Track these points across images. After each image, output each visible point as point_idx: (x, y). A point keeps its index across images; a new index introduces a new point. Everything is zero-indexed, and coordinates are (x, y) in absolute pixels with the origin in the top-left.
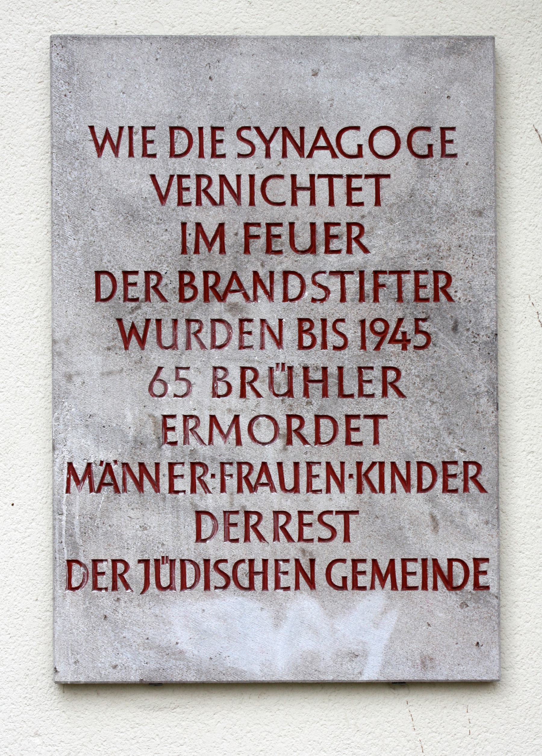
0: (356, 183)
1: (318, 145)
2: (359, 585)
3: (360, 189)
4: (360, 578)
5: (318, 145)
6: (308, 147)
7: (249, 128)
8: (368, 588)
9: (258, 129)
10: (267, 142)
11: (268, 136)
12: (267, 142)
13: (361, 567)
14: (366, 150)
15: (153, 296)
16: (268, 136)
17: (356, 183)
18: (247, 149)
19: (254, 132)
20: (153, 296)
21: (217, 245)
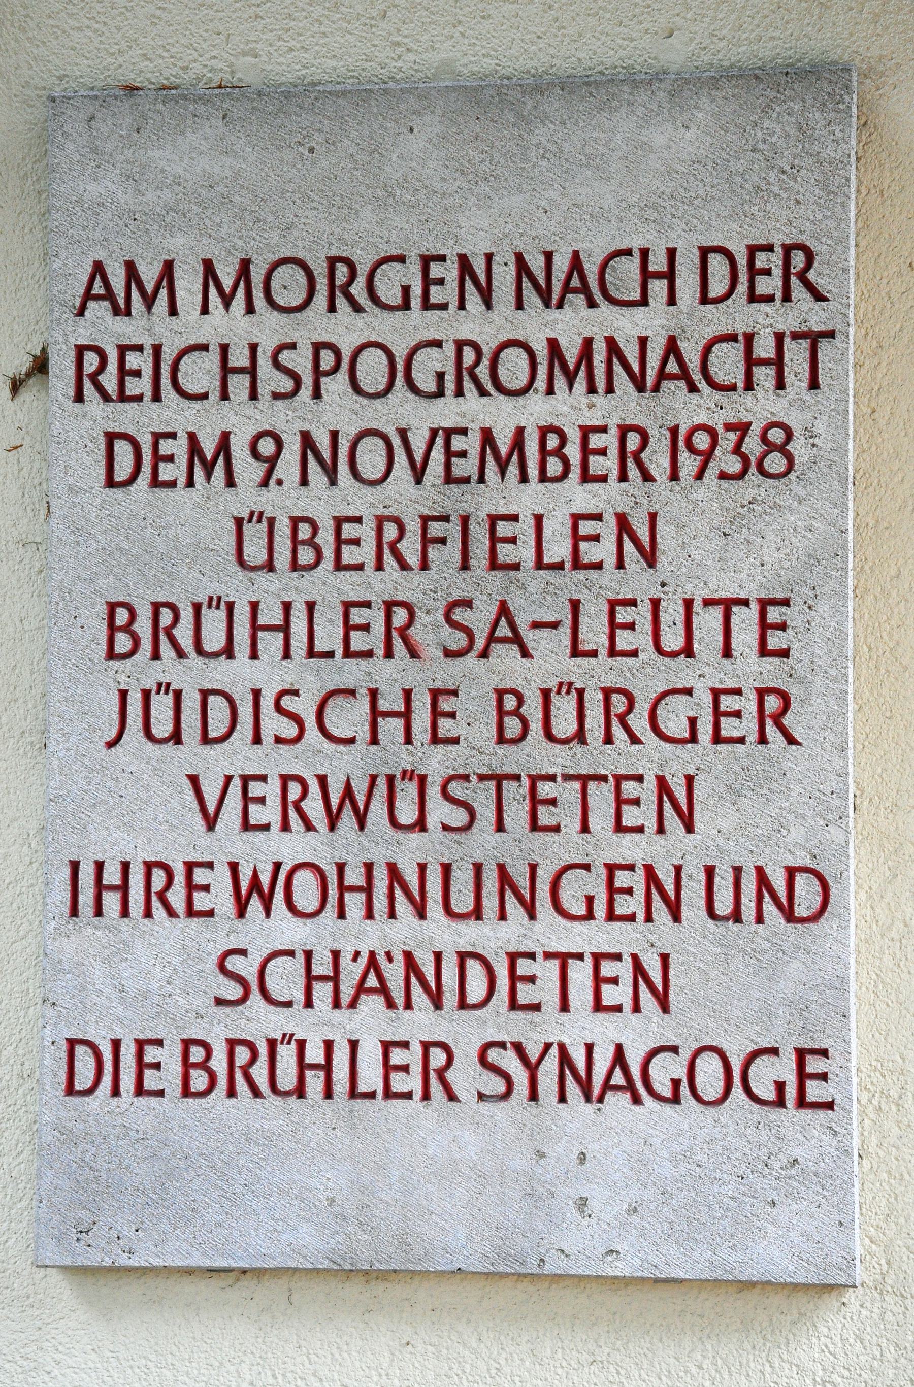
0: (545, 790)
1: (612, 1082)
2: (808, 1100)
3: (553, 802)
4: (760, 280)
5: (612, 1082)
6: (596, 1091)
7: (502, 1045)
8: (567, 565)
9: (519, 1048)
10: (532, 1069)
11: (533, 1059)
12: (532, 1069)
13: (622, 879)
14: (685, 1090)
15: (798, 289)
16: (533, 1059)
17: (545, 790)
18: (498, 1085)
19: (511, 1053)
20: (798, 289)
21: (513, 470)
